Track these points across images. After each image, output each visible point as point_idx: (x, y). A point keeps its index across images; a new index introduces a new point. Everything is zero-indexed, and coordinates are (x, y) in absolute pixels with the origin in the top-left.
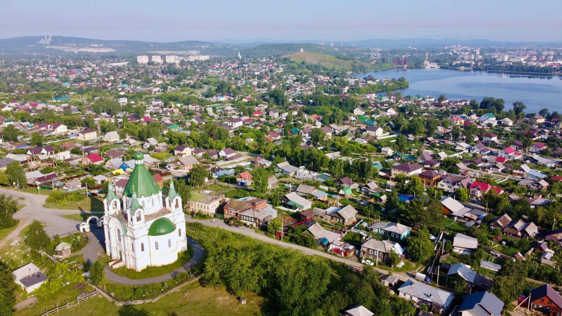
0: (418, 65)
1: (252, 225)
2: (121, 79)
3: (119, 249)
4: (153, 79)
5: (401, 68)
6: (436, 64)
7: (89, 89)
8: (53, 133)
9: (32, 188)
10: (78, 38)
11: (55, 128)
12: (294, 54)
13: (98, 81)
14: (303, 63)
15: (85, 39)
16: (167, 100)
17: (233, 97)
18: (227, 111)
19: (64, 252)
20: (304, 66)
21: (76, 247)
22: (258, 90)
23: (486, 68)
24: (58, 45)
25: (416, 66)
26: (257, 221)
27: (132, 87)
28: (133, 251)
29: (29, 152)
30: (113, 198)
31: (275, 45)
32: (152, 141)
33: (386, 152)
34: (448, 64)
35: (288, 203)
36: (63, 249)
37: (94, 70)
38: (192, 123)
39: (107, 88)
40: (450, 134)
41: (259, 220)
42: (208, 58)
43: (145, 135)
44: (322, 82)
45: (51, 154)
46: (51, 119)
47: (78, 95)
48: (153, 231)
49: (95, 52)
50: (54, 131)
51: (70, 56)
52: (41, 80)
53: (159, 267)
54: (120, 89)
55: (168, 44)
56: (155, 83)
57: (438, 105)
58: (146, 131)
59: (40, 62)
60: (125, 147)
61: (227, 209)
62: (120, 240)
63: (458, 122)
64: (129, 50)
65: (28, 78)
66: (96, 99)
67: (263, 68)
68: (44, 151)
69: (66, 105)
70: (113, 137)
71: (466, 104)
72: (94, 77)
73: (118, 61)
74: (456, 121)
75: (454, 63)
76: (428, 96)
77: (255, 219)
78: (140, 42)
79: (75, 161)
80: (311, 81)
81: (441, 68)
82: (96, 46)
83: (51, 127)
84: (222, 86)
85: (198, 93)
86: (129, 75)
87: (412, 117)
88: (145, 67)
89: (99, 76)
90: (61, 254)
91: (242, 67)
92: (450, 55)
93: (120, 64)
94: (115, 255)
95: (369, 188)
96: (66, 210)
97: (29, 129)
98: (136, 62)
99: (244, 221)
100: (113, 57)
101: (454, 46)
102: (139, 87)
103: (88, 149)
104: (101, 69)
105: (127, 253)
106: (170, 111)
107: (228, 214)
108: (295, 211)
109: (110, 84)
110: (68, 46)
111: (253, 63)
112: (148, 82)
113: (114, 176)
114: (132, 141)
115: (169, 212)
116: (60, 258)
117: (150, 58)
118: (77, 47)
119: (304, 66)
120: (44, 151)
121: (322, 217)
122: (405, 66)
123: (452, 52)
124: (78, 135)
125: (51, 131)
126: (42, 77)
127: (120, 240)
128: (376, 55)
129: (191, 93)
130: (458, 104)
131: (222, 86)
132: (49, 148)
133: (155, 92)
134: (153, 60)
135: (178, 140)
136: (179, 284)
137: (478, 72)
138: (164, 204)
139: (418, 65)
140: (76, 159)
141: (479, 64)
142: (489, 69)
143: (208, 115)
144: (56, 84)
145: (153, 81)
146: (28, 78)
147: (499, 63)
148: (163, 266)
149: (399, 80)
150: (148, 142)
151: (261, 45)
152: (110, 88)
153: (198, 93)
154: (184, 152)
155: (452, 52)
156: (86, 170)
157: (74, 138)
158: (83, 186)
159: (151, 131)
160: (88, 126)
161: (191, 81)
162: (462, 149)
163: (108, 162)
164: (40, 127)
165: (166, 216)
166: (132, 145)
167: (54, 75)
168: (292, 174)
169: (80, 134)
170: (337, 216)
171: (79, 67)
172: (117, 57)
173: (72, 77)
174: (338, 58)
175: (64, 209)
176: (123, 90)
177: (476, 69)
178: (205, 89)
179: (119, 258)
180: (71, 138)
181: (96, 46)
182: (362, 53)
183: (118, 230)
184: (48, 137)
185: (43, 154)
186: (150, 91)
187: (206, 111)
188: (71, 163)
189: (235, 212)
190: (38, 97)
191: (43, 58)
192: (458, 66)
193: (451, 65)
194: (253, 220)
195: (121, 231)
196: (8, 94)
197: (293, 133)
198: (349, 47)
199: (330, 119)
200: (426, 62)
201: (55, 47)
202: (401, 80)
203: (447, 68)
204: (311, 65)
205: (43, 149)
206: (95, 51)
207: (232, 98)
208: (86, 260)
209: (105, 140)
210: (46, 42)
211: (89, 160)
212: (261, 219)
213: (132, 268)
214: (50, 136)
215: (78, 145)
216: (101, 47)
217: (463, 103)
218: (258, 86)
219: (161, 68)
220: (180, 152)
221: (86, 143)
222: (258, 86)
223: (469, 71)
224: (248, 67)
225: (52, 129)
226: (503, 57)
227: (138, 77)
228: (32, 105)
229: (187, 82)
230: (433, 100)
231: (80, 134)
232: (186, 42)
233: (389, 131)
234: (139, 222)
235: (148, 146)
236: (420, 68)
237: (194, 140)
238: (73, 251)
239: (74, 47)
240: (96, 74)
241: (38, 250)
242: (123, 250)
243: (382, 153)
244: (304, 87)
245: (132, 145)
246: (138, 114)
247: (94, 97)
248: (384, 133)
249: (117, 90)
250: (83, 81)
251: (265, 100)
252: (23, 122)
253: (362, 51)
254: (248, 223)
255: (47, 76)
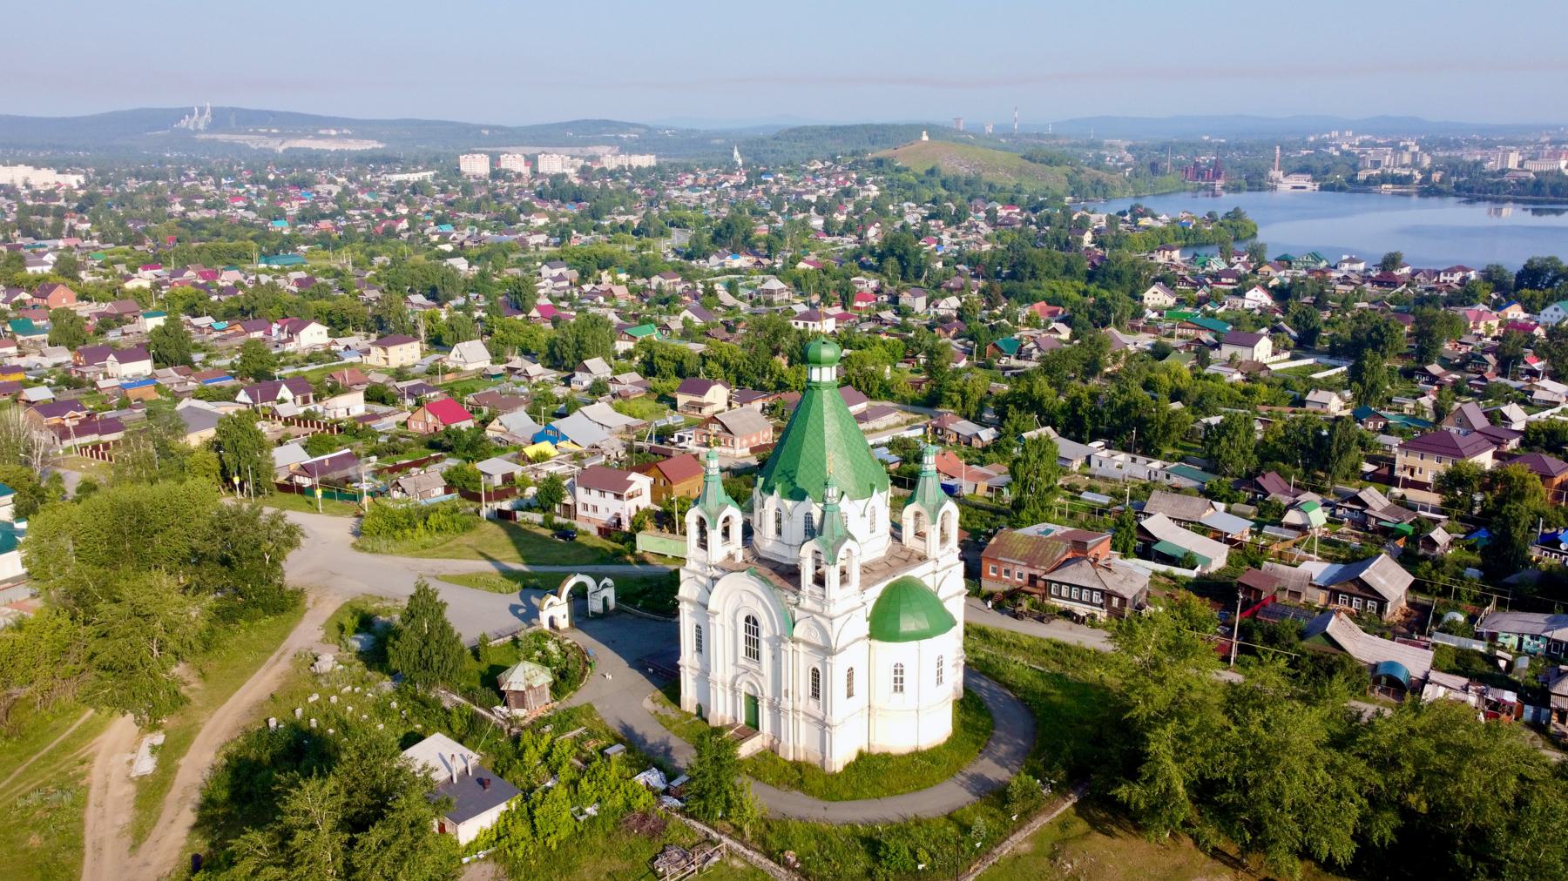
0: (1256, 181)
1: (1093, 616)
2: (428, 213)
3: (744, 688)
4: (520, 211)
5: (1206, 188)
6: (1309, 177)
7: (348, 237)
8: (290, 347)
9: (288, 497)
10: (282, 114)
11: (294, 332)
12: (901, 150)
13: (367, 217)
14: (931, 172)
15: (303, 116)
16: (588, 265)
17: (768, 257)
18: (771, 292)
19: (530, 698)
20: (937, 181)
21: (564, 680)
22: (829, 240)
23: (1458, 187)
24: (231, 132)
25: (1250, 184)
26: (1115, 602)
27: (467, 232)
28: (816, 695)
29: (242, 396)
30: (723, 506)
31: (833, 128)
32: (598, 367)
33: (1323, 405)
34: (1343, 179)
35: (1156, 547)
36: (530, 687)
37: (345, 188)
38: (686, 322)
39: (398, 236)
40: (1490, 358)
41: (1123, 600)
42: (653, 163)
43: (569, 353)
44: (1009, 222)
45: (306, 401)
46: (276, 310)
47: (322, 253)
48: (883, 625)
49: (333, 148)
50: (290, 340)
51: (267, 158)
52: (206, 214)
53: (902, 757)
54: (435, 238)
55: (525, 129)
56: (527, 222)
57: (1387, 280)
58: (571, 340)
59: (192, 174)
60: (518, 385)
61: (994, 560)
62: (754, 654)
63: (1482, 324)
64: (441, 143)
65: (168, 210)
66: (378, 260)
67: (819, 187)
68: (285, 392)
69: (302, 275)
70: (472, 356)
71: (1464, 280)
72: (351, 207)
73: (404, 171)
74: (1476, 322)
75: (1362, 176)
76: (1345, 257)
77: (1107, 595)
78: (452, 123)
79: (386, 420)
80: (978, 218)
81: (1321, 188)
82: (333, 132)
83: (281, 330)
84: (728, 227)
85: (665, 247)
86: (450, 204)
87: (1328, 314)
88: (486, 183)
89: (367, 206)
90: (521, 703)
91: (759, 182)
92: (1332, 157)
93: (414, 177)
94: (724, 710)
95: (1366, 505)
96: (441, 561)
97: (216, 335)
98: (458, 172)
99: (1061, 604)
100: (387, 161)
101: (1335, 134)
102: (486, 233)
103: (415, 387)
104: (368, 188)
105: (787, 704)
106: (602, 293)
107: (999, 578)
108: (1193, 574)
109: (404, 224)
110: (256, 133)
111: (788, 172)
112: (508, 220)
113: (530, 461)
114: (535, 370)
115: (923, 558)
116: (517, 719)
117: (494, 160)
118: (283, 136)
119: (937, 181)
120: (285, 392)
121: (1297, 595)
122: (1219, 184)
123: (1338, 148)
124: (368, 352)
125: (283, 342)
126: (207, 207)
127: (754, 654)
128: (1118, 154)
129: (641, 248)
130: (1442, 277)
131: (728, 227)
132: (298, 385)
133: (537, 246)
134: (503, 166)
135: (673, 365)
136: (1019, 826)
137: (1434, 200)
138: (896, 528)
139: (1256, 181)
140: (387, 414)
141: (1436, 176)
142: (1470, 190)
143: (720, 304)
144: (251, 225)
145: (522, 217)
146: (168, 210)
147: (1494, 175)
148: (917, 754)
149: (1227, 215)
150: (587, 370)
151: (794, 130)
152: (405, 235)
153: (665, 247)
154: (707, 398)
155: (1338, 148)
156: (433, 446)
157: (356, 359)
158: (448, 491)
159: (588, 340)
160: (386, 328)
161: (631, 218)
162: (1555, 399)
163: (494, 425)
164: (247, 331)
165: (916, 572)
166: (534, 381)
167: (241, 203)
168: (1076, 465)
169: (373, 349)
170: (1355, 590)
171: (302, 184)
172: (397, 160)
173: (293, 208)
174: (1030, 159)
175: (430, 556)
176: (444, 238)
177: (1429, 191)
178: (679, 238)
179: (742, 720)
180: (347, 360)
181: (333, 132)
182: (1077, 151)
183: (751, 621)
184: (278, 356)
185: (283, 401)
186: (523, 242)
187: (554, 442)
188: (377, 425)
189: (1027, 571)
190: (217, 256)
191: (195, 163)
192: (1375, 184)
193: (1352, 180)
194: (1097, 598)
195: (764, 621)
196: (127, 247)
197: (1001, 351)
198: (1039, 136)
199: (1092, 316)
200: (1276, 174)
201: (223, 137)
202: (1236, 215)
203: (1341, 189)
204: (957, 178)
205: (284, 387)
206: (333, 146)
207: (766, 262)
208: (618, 731)
209: (451, 365)
210: (196, 123)
211: (430, 418)
212: (1129, 597)
213: (802, 757)
214: (283, 354)
215: (379, 379)
216: (347, 136)
217: (1457, 277)
218: (827, 231)
219: (531, 186)
220: (696, 399)
221: (400, 374)
222: (827, 231)
223: (1407, 195)
224: (776, 182)
225: (284, 336)
226: (1505, 159)
227: (477, 208)
228: (203, 275)
229: (621, 219)
230: (1361, 266)
231: (373, 349)
232: (577, 122)
233: (1286, 348)
234: (847, 589)
235: (587, 383)
236: (1261, 188)
237: (726, 366)
238: (556, 690)
239: (275, 135)
240: (356, 200)
241: (429, 688)
242: (768, 693)
243: (1309, 407)
244: (959, 233)
245: (534, 381)
246: (519, 299)
247: (373, 255)
248: (1275, 353)
249: (427, 240)
250: (324, 217)
251: (863, 266)
252: (195, 316)
253: (1077, 145)
254: (1081, 610)
255: (223, 205)
